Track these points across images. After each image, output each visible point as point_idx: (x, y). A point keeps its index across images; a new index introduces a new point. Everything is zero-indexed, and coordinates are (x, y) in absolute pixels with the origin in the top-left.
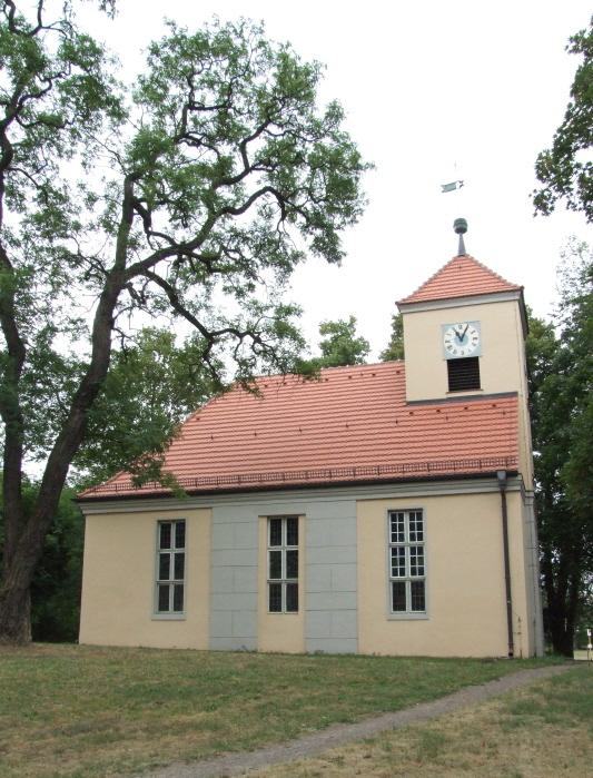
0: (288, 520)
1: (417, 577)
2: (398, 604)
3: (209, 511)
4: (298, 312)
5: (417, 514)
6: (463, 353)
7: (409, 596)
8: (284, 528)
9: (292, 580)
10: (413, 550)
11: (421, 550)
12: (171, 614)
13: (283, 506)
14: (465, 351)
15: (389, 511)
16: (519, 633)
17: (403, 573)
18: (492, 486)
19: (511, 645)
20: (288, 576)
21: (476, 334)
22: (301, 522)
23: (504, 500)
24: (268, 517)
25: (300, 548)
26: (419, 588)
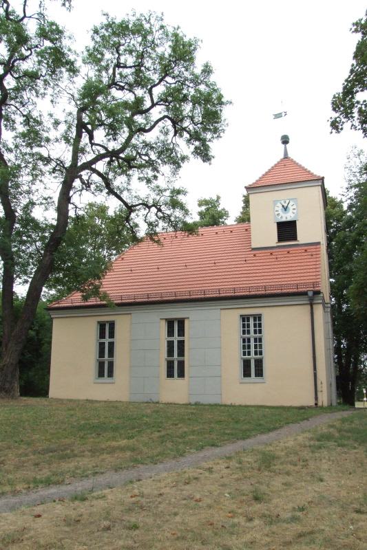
0: (178, 322)
1: (258, 356)
2: (247, 373)
3: (130, 315)
4: (185, 193)
5: (258, 318)
6: (286, 218)
7: (253, 368)
8: (176, 326)
9: (181, 358)
10: (255, 340)
11: (260, 340)
12: (106, 379)
13: (175, 313)
14: (288, 217)
15: (241, 316)
16: (321, 391)
17: (249, 354)
18: (304, 300)
19: (316, 398)
20: (178, 356)
22: (186, 322)
23: (312, 309)
24: (166, 319)
25: (186, 338)
26: (259, 363)
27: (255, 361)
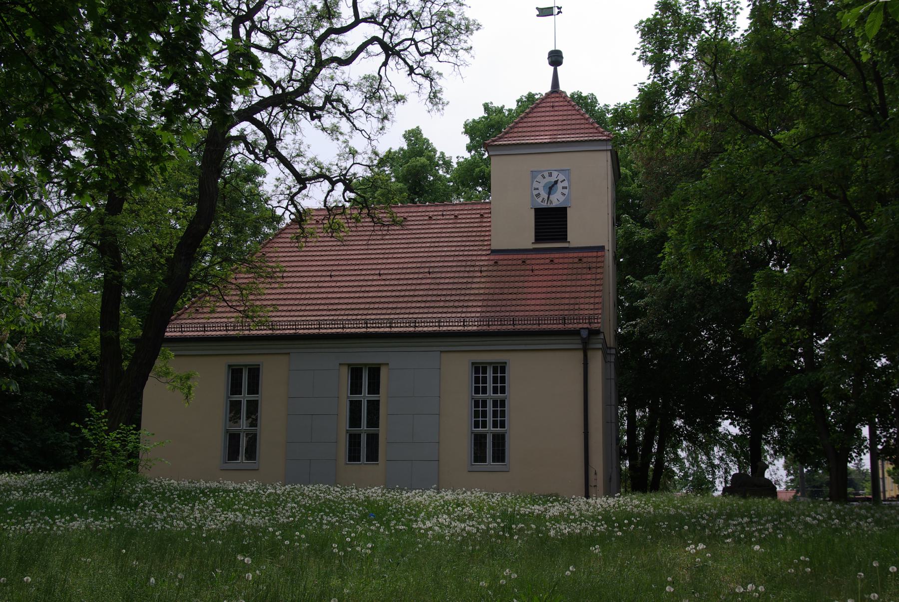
0: (250, 370)
1: (499, 429)
10: (495, 403)
11: (503, 403)
21: (565, 184)
24: (349, 365)
27: (494, 436)
